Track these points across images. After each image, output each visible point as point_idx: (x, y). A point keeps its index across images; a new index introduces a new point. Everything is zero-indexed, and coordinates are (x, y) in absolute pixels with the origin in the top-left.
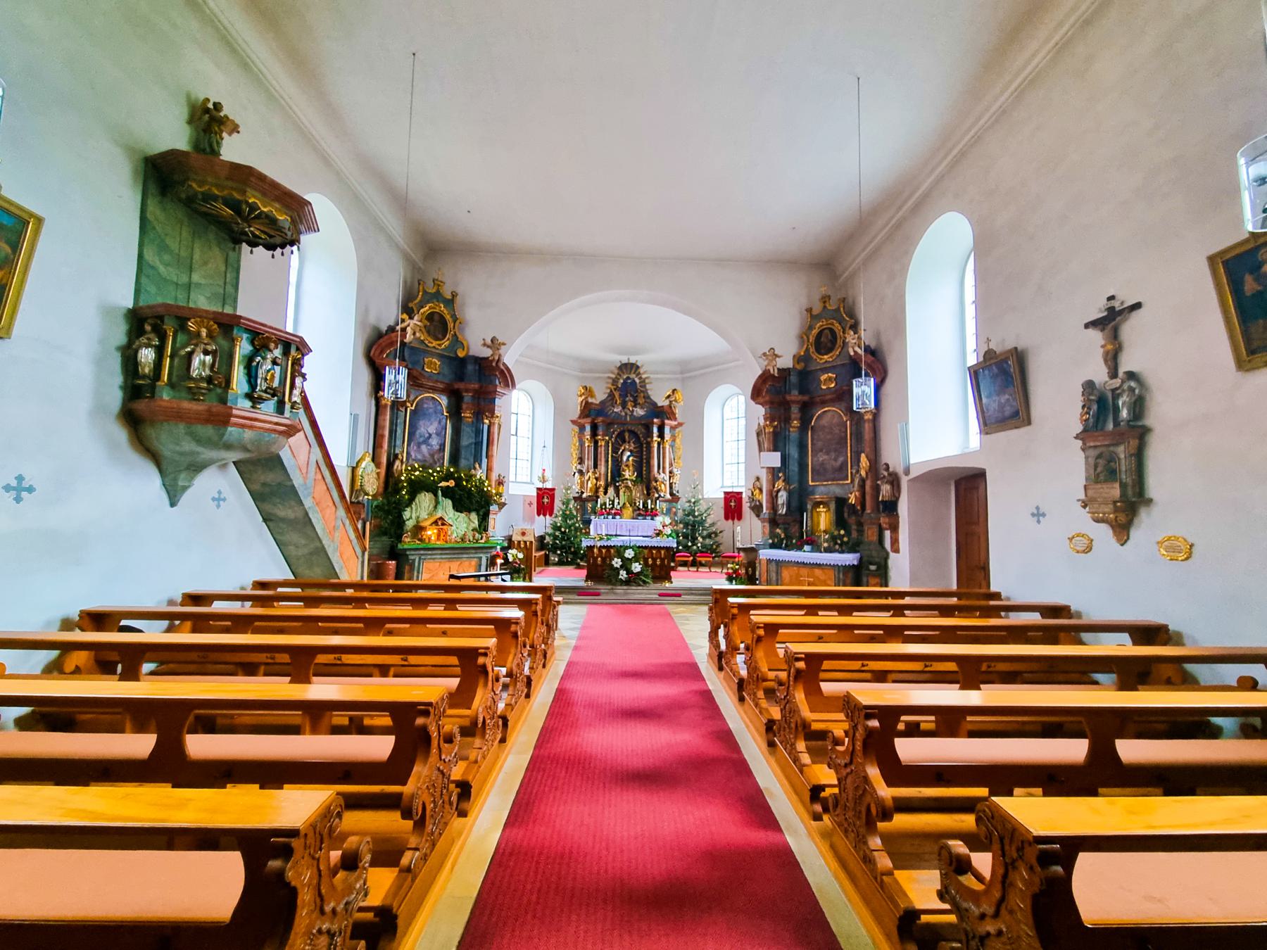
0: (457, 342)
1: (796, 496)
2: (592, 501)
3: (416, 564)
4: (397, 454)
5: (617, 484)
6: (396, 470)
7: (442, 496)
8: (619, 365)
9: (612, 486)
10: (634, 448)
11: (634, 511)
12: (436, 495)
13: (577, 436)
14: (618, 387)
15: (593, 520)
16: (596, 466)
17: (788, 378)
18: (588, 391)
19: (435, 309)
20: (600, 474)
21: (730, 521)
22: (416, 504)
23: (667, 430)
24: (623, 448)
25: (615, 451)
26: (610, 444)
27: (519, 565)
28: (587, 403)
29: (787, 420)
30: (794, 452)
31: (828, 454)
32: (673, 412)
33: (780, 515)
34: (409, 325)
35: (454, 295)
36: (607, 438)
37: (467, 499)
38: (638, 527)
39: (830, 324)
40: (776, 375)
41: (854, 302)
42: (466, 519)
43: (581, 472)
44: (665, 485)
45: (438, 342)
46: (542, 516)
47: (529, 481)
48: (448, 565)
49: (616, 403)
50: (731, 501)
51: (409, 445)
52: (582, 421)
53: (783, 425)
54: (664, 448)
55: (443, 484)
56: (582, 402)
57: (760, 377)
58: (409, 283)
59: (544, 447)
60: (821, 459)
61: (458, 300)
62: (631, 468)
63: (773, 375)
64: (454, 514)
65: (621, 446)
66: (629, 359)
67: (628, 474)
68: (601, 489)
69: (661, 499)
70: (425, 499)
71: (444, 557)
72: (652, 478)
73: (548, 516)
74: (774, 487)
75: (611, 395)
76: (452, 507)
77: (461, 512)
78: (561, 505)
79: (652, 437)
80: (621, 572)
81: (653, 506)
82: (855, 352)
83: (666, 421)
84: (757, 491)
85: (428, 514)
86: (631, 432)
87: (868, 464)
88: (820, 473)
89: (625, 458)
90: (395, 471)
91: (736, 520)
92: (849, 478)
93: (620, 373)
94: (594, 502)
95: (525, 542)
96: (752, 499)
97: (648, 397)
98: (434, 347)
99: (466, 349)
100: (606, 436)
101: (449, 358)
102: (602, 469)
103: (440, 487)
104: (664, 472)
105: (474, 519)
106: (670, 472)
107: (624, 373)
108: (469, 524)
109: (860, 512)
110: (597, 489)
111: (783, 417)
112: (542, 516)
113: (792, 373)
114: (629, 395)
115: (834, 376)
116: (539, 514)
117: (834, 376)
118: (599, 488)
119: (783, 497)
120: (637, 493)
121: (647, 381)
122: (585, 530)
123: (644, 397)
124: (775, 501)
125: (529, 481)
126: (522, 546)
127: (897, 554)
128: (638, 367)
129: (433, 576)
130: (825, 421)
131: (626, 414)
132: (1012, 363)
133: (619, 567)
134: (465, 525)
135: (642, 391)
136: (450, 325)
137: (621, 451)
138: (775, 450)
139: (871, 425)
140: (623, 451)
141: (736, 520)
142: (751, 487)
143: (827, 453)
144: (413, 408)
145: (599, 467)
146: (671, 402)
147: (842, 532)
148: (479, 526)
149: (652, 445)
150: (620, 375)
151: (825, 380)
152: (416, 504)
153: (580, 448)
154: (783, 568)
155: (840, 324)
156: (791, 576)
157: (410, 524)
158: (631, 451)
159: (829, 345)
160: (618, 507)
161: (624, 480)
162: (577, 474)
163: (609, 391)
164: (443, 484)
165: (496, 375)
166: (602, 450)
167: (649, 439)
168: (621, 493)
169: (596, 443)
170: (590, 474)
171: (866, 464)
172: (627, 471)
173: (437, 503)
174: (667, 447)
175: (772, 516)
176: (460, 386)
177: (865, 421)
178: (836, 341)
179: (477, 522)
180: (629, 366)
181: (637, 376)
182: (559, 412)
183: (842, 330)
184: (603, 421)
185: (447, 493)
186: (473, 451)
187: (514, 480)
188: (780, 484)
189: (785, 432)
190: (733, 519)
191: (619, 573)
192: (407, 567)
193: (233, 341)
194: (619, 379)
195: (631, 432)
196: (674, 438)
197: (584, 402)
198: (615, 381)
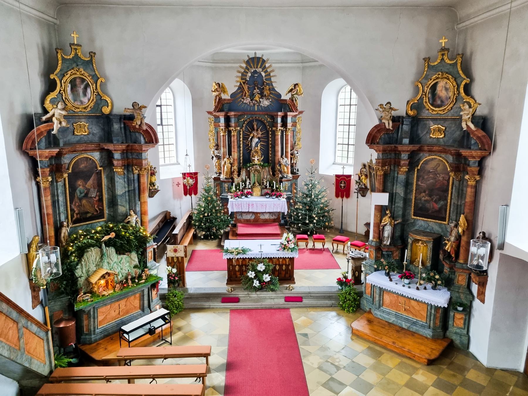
0: (100, 101)
1: (398, 229)
2: (229, 182)
3: (92, 313)
4: (63, 222)
5: (248, 169)
6: (64, 237)
7: (106, 246)
8: (246, 59)
9: (244, 169)
10: (262, 134)
11: (262, 189)
12: (100, 247)
13: (213, 124)
14: (246, 80)
15: (230, 200)
16: (230, 154)
17: (401, 126)
18: (221, 88)
19: (76, 74)
20: (234, 160)
21: (340, 198)
22: (85, 260)
23: (289, 120)
24: (252, 135)
25: (245, 138)
26: (241, 133)
27: (174, 278)
28: (220, 99)
29: (397, 164)
30: (400, 190)
32: (294, 104)
33: (385, 245)
34: (53, 115)
35: (92, 54)
36: (239, 128)
37: (127, 244)
38: (266, 205)
40: (391, 129)
41: (471, 54)
42: (128, 259)
43: (219, 158)
44: (287, 168)
46: (188, 195)
47: (176, 162)
49: (245, 96)
50: (341, 183)
51: (71, 202)
52: (217, 114)
53: (392, 168)
54: (287, 136)
55: (106, 238)
56: (216, 97)
57: (376, 127)
58: (47, 52)
59: (187, 155)
61: (95, 60)
62: (260, 153)
63: (389, 129)
64: (118, 258)
65: (251, 133)
66: (255, 53)
67: (257, 159)
68: (235, 173)
69: (284, 179)
70: (93, 254)
72: (277, 161)
73: (193, 195)
74: (381, 222)
75: (241, 88)
76: (115, 253)
77: (124, 254)
78: (203, 192)
79: (277, 127)
80: (255, 281)
81: (277, 186)
82: (468, 126)
83: (289, 113)
84: (363, 177)
85: (97, 265)
86: (257, 120)
87: (466, 225)
88: (421, 212)
89: (254, 144)
90: (63, 239)
91: (345, 198)
93: (248, 67)
94: (230, 184)
95: (178, 258)
96: (359, 182)
97: (274, 89)
99: (110, 104)
100: (238, 127)
101: (97, 117)
102: (235, 155)
104: (286, 157)
105: (135, 257)
106: (292, 154)
107: (251, 67)
108: (131, 263)
109: (454, 259)
110: (232, 173)
111: (393, 161)
112: (188, 195)
113: (405, 123)
114: (256, 88)
115: (444, 128)
116: (186, 194)
117: (444, 128)
118: (234, 172)
119: (388, 232)
120: (266, 174)
121: (272, 74)
122: (224, 210)
123: (269, 90)
124: (381, 233)
125: (176, 162)
126: (175, 261)
128: (264, 61)
130: (430, 167)
131: (254, 105)
133: (253, 277)
134: (128, 264)
135: (267, 84)
137: (250, 137)
138: (384, 191)
139: (473, 190)
140: (252, 137)
141: (345, 198)
142: (359, 173)
145: (232, 153)
146: (292, 95)
147: (437, 277)
148: (140, 262)
149: (276, 134)
150: (248, 70)
151: (434, 130)
152: (85, 260)
153: (216, 135)
155: (455, 80)
157: (81, 281)
158: (259, 138)
160: (250, 186)
161: (253, 165)
162: (215, 158)
163: (238, 84)
166: (234, 139)
167: (274, 129)
168: (252, 175)
169: (230, 132)
170: (226, 159)
171: (464, 224)
172: (256, 157)
173: (102, 255)
174: (289, 134)
175: (378, 245)
176: (110, 147)
177: (467, 186)
179: (137, 260)
180: (256, 61)
181: (263, 70)
182: (196, 103)
183: (456, 86)
184: (235, 115)
185: (108, 244)
186: (127, 197)
187: (163, 163)
188: (386, 220)
189: (394, 174)
190: (342, 197)
191: (253, 282)
192: (84, 316)
194: (247, 73)
195: (257, 120)
196: (294, 124)
197: (218, 98)
198: (244, 75)
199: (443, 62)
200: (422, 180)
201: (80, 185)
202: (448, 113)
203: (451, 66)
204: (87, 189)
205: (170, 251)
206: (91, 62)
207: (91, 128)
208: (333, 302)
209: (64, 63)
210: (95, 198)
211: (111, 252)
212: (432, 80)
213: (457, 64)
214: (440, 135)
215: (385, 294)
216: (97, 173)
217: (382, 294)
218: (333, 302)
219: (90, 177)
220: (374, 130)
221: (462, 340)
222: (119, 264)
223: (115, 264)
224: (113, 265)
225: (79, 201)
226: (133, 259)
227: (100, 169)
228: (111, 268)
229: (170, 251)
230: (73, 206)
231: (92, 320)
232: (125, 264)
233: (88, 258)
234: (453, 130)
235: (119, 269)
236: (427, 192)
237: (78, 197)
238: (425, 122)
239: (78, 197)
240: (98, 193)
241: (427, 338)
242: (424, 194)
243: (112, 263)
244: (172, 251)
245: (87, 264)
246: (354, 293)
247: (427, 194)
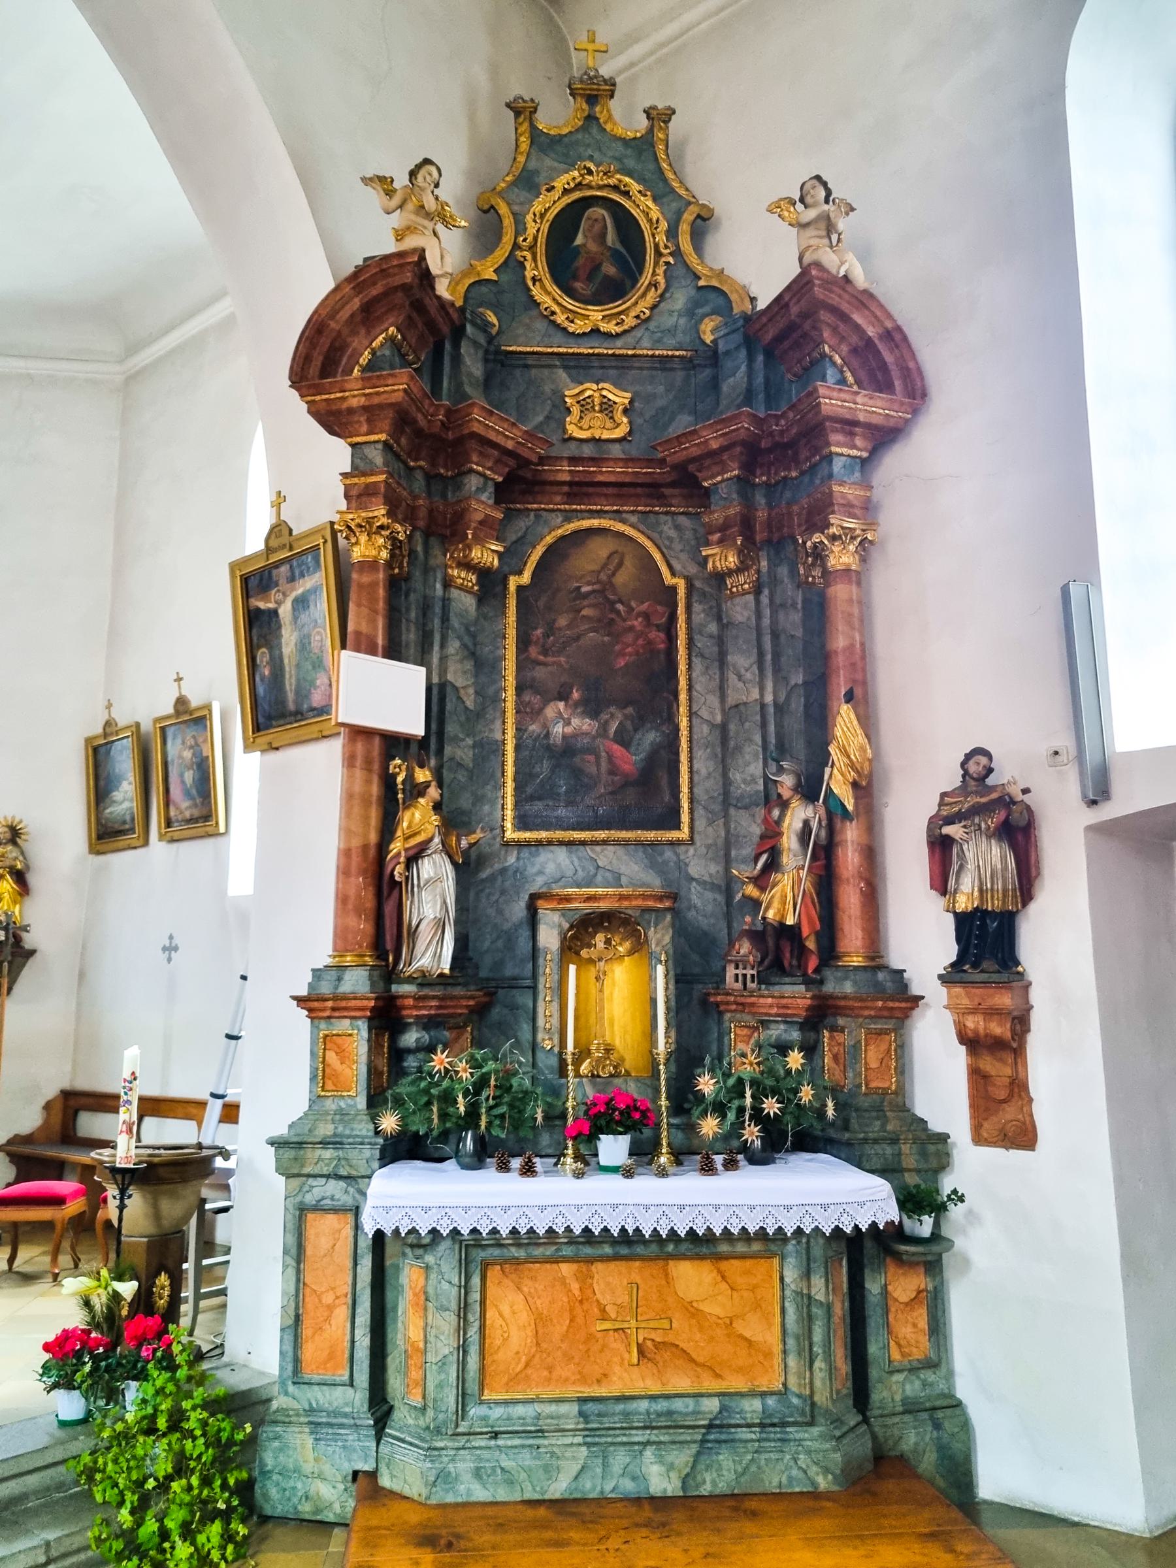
31: (594, 714)
33: (424, 980)
39: (615, 188)
60: (558, 730)
92: (527, 835)
127: (1017, 1156)
136: (655, 237)
143: (592, 707)
154: (494, 1273)
156: (540, 1321)
159: (609, 269)
178: (641, 268)
199: (594, 130)
200: (546, 635)
202: (638, 333)
203: (629, 152)
208: (51, 1535)
212: (556, 194)
213: (652, 145)
214: (609, 424)
215: (492, 1290)
217: (476, 1296)
218: (51, 1535)
220: (345, 302)
221: (946, 1438)
234: (663, 409)
236: (576, 695)
238: (534, 372)
241: (815, 1495)
242: (561, 705)
246: (206, 1405)
247: (576, 704)
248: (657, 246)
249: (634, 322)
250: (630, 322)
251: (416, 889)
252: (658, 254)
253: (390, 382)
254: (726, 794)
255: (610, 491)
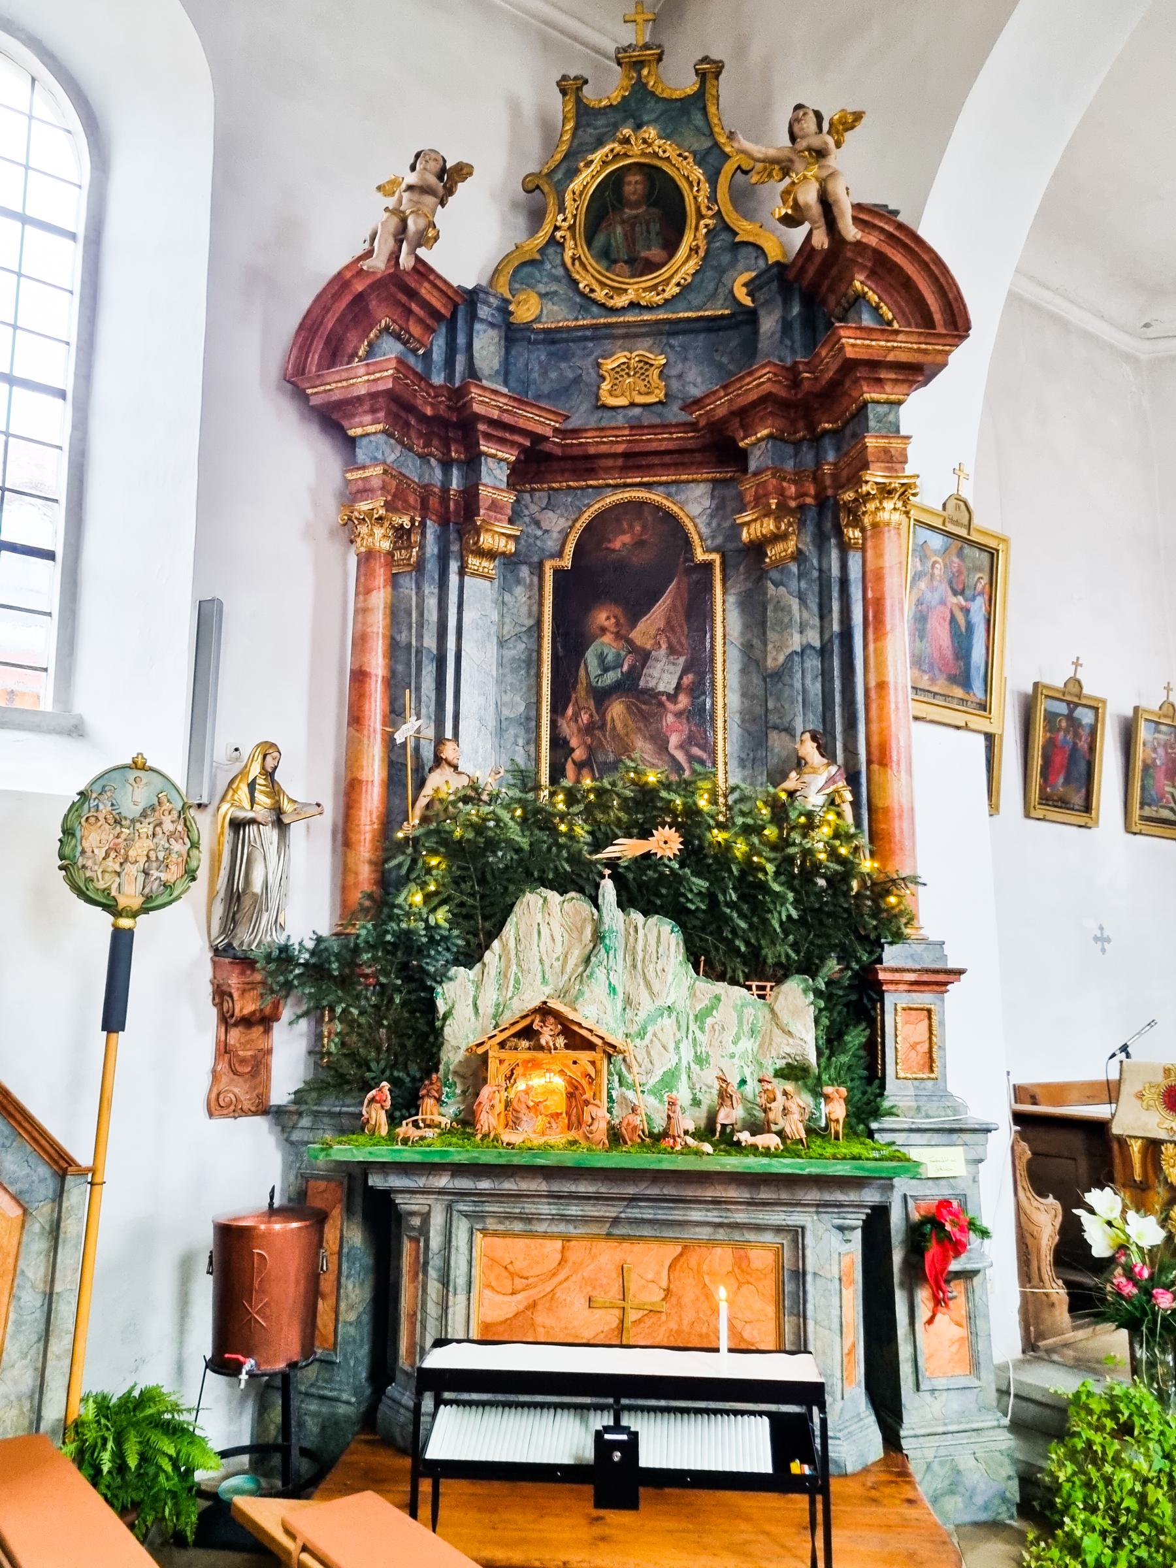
45: (648, 280)
48: (608, 1255)
51: (558, 708)
55: (626, 848)
64: (693, 994)
71: (574, 1210)
98: (633, 305)
103: (612, 863)
105: (796, 1013)
129: (533, 1305)
132: (625, 904)
136: (696, 195)
144: (567, 562)
152: (504, 946)
164: (626, 848)
165: (860, 297)
193: (473, 462)
201: (603, 630)
204: (633, 648)
205: (1140, 1096)
206: (698, 101)
207: (680, 376)
209: (589, 125)
210: (673, 697)
211: (652, 941)
216: (689, 571)
219: (653, 597)
222: (693, 1027)
223: (667, 1022)
224: (651, 1019)
225: (592, 704)
226: (784, 1018)
227: (700, 556)
228: (634, 1029)
229: (1140, 1096)
230: (568, 729)
231: (434, 1287)
232: (728, 1037)
233: (518, 941)
235: (687, 1053)
237: (589, 684)
239: (589, 684)
240: (688, 679)
243: (647, 1006)
244: (1153, 1097)
245: (508, 967)
248: (698, 209)
249: (677, 290)
250: (672, 290)
251: (611, 1212)
252: (700, 216)
253: (318, 383)
254: (766, 722)
255: (667, 459)
